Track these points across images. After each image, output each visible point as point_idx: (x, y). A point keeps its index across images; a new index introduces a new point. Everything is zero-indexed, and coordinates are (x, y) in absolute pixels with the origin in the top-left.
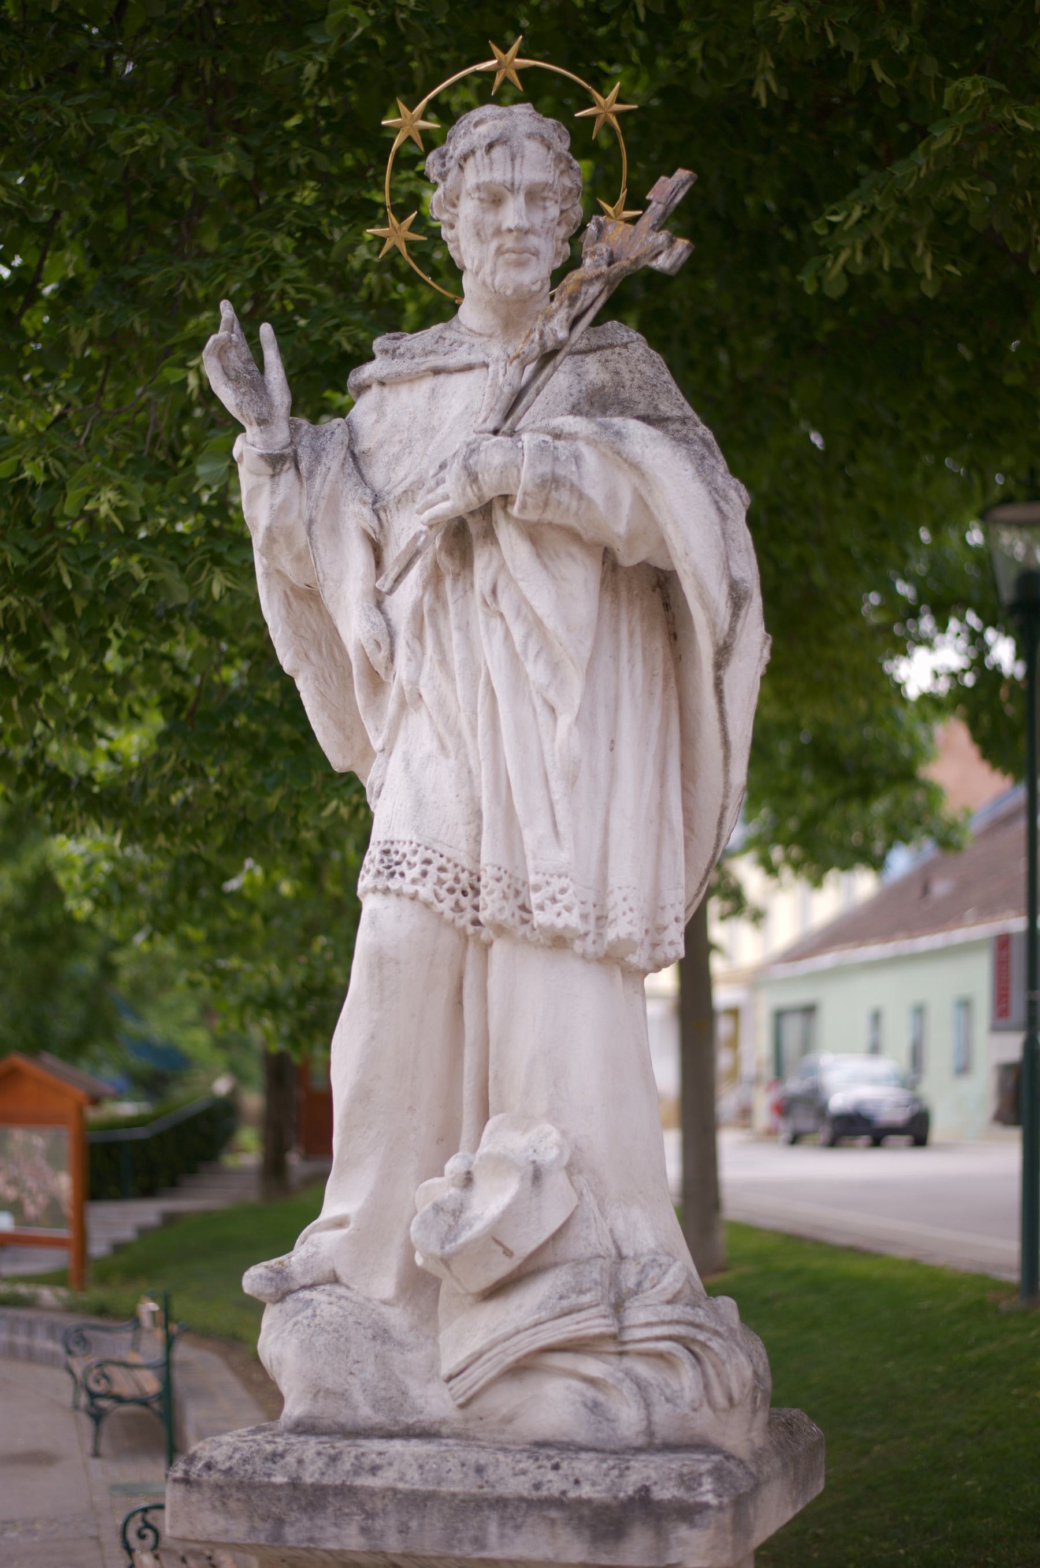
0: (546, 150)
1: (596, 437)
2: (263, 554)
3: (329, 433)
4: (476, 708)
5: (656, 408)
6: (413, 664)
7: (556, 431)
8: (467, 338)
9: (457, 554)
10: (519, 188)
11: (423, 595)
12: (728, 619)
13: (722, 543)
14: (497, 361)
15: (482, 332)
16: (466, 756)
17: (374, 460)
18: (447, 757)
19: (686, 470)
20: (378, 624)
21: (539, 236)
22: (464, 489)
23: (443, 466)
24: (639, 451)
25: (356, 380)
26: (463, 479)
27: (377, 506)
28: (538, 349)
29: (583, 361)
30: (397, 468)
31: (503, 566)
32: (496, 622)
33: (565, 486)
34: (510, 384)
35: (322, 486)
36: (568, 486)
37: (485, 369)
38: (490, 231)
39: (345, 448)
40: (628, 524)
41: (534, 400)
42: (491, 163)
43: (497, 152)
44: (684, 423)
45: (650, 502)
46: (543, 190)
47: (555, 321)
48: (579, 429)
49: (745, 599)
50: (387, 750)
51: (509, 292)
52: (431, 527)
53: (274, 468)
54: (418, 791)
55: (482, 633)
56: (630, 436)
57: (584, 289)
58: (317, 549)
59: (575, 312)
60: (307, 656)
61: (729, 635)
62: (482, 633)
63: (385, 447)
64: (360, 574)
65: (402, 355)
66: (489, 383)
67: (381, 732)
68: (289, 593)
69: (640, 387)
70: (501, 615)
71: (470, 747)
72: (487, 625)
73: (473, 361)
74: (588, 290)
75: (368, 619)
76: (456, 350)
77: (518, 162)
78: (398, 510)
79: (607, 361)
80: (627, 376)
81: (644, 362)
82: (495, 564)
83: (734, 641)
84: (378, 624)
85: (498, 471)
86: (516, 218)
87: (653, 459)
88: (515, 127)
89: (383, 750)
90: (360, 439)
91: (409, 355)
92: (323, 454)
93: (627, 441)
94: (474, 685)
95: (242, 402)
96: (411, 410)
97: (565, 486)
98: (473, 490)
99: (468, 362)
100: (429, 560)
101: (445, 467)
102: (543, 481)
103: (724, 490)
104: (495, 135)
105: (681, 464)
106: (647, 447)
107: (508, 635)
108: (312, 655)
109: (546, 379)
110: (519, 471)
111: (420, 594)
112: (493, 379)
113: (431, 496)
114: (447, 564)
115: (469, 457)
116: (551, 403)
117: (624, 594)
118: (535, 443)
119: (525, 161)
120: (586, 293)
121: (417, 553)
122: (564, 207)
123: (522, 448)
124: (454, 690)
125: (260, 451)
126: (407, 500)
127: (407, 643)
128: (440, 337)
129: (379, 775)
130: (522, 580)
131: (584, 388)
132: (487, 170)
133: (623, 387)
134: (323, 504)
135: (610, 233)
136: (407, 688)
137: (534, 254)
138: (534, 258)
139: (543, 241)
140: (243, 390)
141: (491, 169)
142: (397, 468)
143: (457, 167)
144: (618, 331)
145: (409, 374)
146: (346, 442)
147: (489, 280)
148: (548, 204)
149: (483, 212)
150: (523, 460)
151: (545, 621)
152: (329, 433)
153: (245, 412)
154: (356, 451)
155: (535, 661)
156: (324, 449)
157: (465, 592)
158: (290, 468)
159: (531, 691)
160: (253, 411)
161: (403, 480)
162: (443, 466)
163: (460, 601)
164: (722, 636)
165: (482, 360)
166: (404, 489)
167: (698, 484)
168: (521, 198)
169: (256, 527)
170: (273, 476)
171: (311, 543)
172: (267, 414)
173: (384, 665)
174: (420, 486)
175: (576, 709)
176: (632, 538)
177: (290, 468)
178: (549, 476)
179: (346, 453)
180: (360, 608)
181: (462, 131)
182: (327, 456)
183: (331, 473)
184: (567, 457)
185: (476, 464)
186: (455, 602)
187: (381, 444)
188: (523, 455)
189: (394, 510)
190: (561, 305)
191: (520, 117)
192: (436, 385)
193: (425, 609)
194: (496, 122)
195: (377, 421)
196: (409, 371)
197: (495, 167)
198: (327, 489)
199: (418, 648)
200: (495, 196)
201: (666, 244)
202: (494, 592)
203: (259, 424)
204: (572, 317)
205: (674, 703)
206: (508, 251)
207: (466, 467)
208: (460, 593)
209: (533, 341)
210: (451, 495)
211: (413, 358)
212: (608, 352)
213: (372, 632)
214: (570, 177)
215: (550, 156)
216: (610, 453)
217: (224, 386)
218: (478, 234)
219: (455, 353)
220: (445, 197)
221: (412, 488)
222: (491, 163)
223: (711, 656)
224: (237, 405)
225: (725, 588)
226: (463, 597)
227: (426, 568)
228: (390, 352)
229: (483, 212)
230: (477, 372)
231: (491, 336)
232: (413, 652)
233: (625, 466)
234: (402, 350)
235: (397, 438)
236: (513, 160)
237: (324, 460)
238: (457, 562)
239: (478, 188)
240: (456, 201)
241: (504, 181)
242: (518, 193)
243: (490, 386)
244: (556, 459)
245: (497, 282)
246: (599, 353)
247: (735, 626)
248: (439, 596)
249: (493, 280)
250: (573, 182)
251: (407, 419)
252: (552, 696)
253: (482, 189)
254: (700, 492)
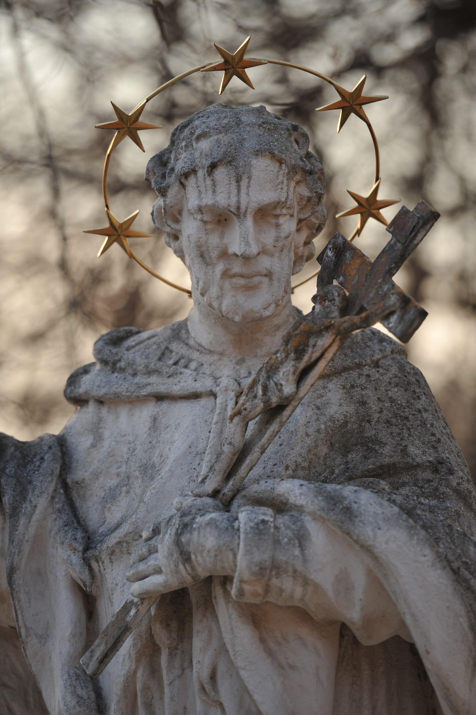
0: (278, 164)
1: (323, 514)
5: (404, 451)
8: (195, 355)
9: (174, 625)
10: (246, 211)
11: (137, 668)
14: (226, 390)
15: (212, 349)
19: (425, 556)
21: (272, 256)
22: (176, 566)
23: (156, 532)
24: (371, 534)
26: (175, 556)
27: (89, 554)
28: (262, 405)
29: (324, 388)
30: (113, 508)
33: (286, 572)
34: (230, 444)
35: (27, 528)
36: (290, 573)
37: (212, 398)
38: (214, 254)
39: (55, 479)
40: (362, 609)
41: (258, 459)
44: (436, 471)
46: (275, 208)
47: (281, 374)
48: (304, 503)
52: (142, 600)
56: (361, 513)
57: (312, 342)
58: (19, 601)
59: (302, 365)
63: (101, 479)
64: (67, 634)
65: (122, 370)
66: (215, 418)
69: (388, 422)
70: (221, 704)
74: (316, 342)
75: (74, 693)
76: (181, 373)
77: (244, 183)
78: (111, 562)
79: (352, 387)
80: (374, 406)
81: (397, 385)
84: (86, 697)
85: (212, 554)
86: (243, 244)
87: (387, 543)
88: (241, 142)
90: (74, 464)
91: (130, 371)
92: (30, 487)
93: (357, 520)
96: (131, 438)
98: (186, 569)
99: (194, 390)
101: (159, 533)
102: (261, 569)
104: (218, 155)
106: (379, 529)
109: (271, 436)
110: (235, 555)
111: (134, 667)
113: (142, 567)
115: (181, 534)
116: (284, 444)
119: (252, 182)
120: (314, 346)
123: (238, 530)
126: (122, 552)
128: (167, 348)
130: (243, 669)
131: (323, 426)
133: (369, 421)
137: (265, 276)
138: (265, 280)
139: (276, 260)
141: (214, 192)
142: (113, 508)
143: (178, 184)
144: (370, 343)
145: (129, 397)
146: (57, 472)
147: (215, 304)
148: (282, 220)
149: (207, 234)
150: (239, 544)
152: (38, 457)
154: (69, 481)
156: (30, 482)
157: (183, 670)
161: (118, 526)
162: (156, 532)
163: (177, 682)
165: (209, 389)
166: (118, 540)
167: (439, 571)
168: (249, 222)
171: (12, 594)
174: (136, 537)
178: (268, 563)
180: (66, 677)
181: (184, 144)
182: (33, 492)
183: (37, 511)
186: (171, 684)
188: (239, 537)
189: (107, 561)
190: (287, 357)
192: (158, 412)
193: (139, 686)
194: (220, 136)
195: (93, 446)
197: (219, 189)
200: (220, 215)
201: (398, 304)
202: (213, 677)
204: (299, 370)
206: (234, 276)
207: (177, 543)
209: (255, 397)
210: (163, 569)
212: (355, 374)
213: (78, 708)
214: (307, 185)
215: (282, 172)
216: (339, 532)
218: (202, 256)
219: (179, 377)
227: (141, 637)
228: (110, 364)
229: (207, 234)
230: (203, 401)
231: (222, 354)
233: (357, 547)
234: (122, 364)
236: (238, 181)
237: (30, 496)
239: (200, 210)
242: (245, 216)
243: (216, 423)
244: (277, 542)
246: (345, 375)
249: (220, 305)
250: (311, 190)
253: (204, 212)
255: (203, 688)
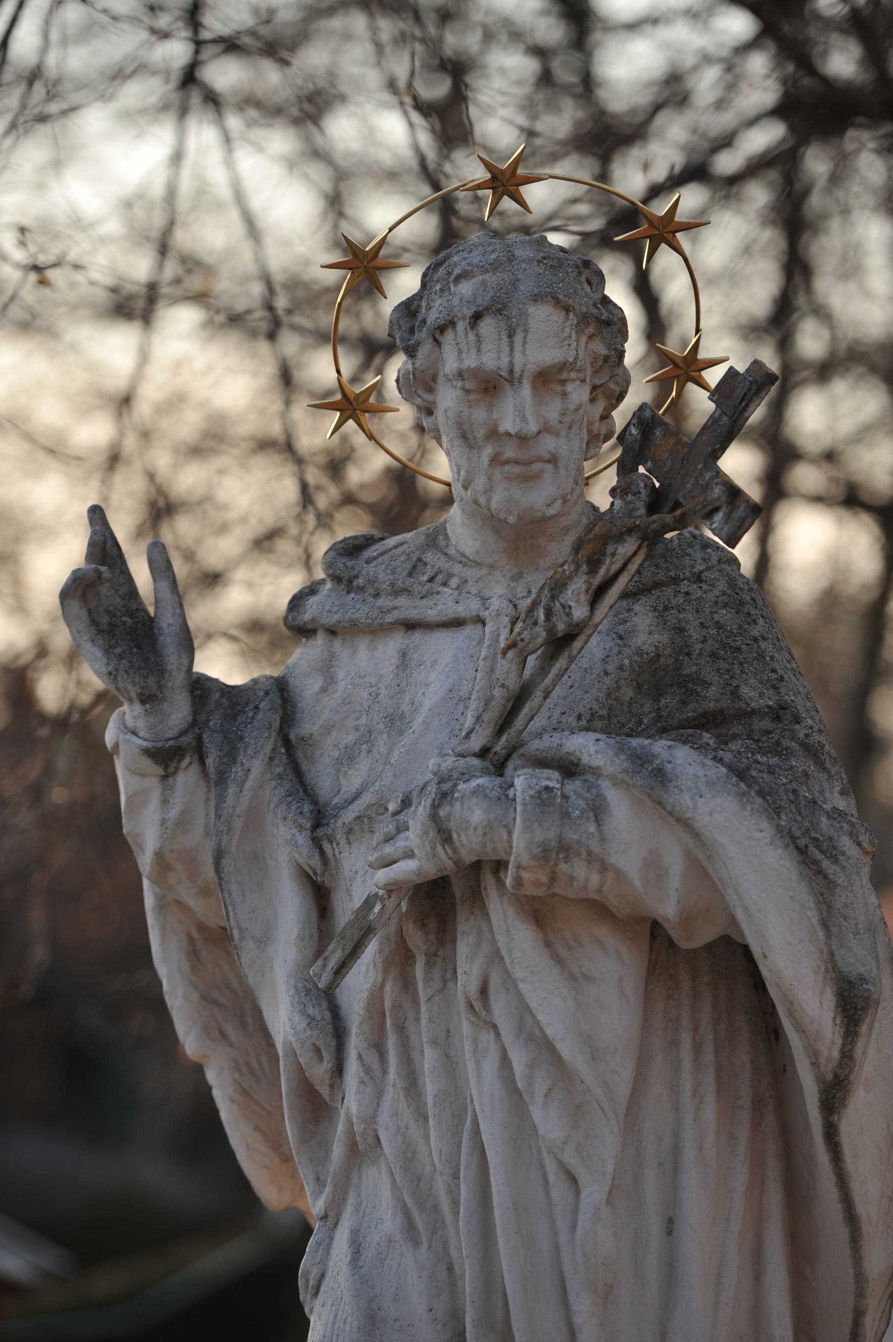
1: (626, 778)
2: (153, 882)
3: (251, 706)
4: (459, 1169)
5: (735, 693)
6: (368, 1090)
7: (572, 758)
8: (457, 568)
9: (432, 924)
12: (839, 1042)
13: (821, 935)
14: (498, 615)
15: (479, 561)
16: (445, 1244)
17: (318, 753)
18: (416, 1243)
19: (761, 831)
20: (319, 1017)
21: (557, 435)
22: (433, 848)
24: (690, 803)
25: (293, 620)
27: (320, 832)
28: (544, 634)
29: (628, 610)
30: (350, 772)
31: (496, 956)
32: (487, 1038)
33: (578, 854)
36: (584, 855)
37: (480, 626)
38: (480, 433)
42: (479, 341)
43: (487, 326)
45: (710, 871)
47: (569, 592)
48: (601, 764)
49: (865, 1009)
50: (332, 1217)
51: (511, 519)
52: (390, 892)
53: (166, 767)
54: (371, 1301)
55: (468, 1054)
57: (610, 549)
58: (230, 894)
59: (597, 580)
60: (223, 1034)
61: (841, 1065)
62: (468, 1054)
63: (334, 734)
64: (293, 937)
65: (361, 589)
67: (324, 1185)
68: (195, 934)
69: (713, 655)
70: (495, 1027)
71: (451, 1230)
72: (475, 1042)
73: (463, 615)
74: (616, 549)
75: (304, 1013)
77: (518, 338)
78: (349, 843)
80: (695, 633)
82: (485, 948)
83: (852, 1070)
84: (319, 1017)
86: (518, 419)
87: (711, 815)
89: (324, 1217)
90: (299, 715)
91: (371, 591)
92: (241, 745)
93: (672, 785)
94: (457, 1134)
95: (117, 670)
96: (373, 680)
97: (578, 854)
100: (392, 928)
101: (410, 805)
102: (544, 851)
103: (831, 838)
104: (483, 301)
105: (753, 822)
107: (505, 1061)
108: (231, 1031)
110: (510, 833)
112: (490, 646)
113: (388, 849)
114: (416, 940)
116: (576, 685)
117: (686, 985)
118: (532, 792)
119: (529, 336)
120: (613, 554)
121: (368, 932)
122: (597, 382)
123: (514, 800)
124: (427, 1138)
125: (145, 744)
127: (360, 1056)
128: (419, 559)
129: (317, 1259)
130: (523, 981)
131: (626, 662)
132: (473, 351)
133: (688, 654)
134: (238, 825)
135: (658, 442)
136: (358, 1128)
137: (549, 461)
138: (549, 467)
139: (563, 440)
140: (118, 650)
141: (479, 350)
143: (430, 340)
146: (276, 725)
147: (482, 500)
148: (569, 387)
149: (470, 407)
150: (515, 819)
151: (559, 1045)
152: (251, 706)
153: (121, 685)
154: (292, 737)
155: (545, 1104)
156: (241, 739)
158: (190, 763)
159: (540, 1148)
160: (134, 684)
161: (357, 796)
162: (406, 803)
163: (437, 998)
164: (830, 1068)
167: (780, 851)
168: (526, 390)
169: (142, 849)
170: (165, 777)
172: (154, 687)
173: (327, 1082)
175: (609, 1179)
176: (687, 918)
177: (190, 763)
179: (276, 740)
181: (438, 287)
182: (245, 751)
183: (251, 777)
184: (582, 812)
185: (449, 815)
187: (328, 729)
188: (515, 810)
189: (343, 842)
191: (523, 266)
192: (408, 645)
193: (387, 1004)
194: (487, 276)
195: (324, 690)
196: (369, 621)
197: (485, 347)
198: (245, 801)
199: (376, 1065)
202: (484, 991)
203: (143, 702)
205: (772, 1147)
206: (508, 462)
207: (434, 817)
208: (437, 985)
209: (535, 623)
210: (416, 852)
211: (377, 596)
212: (669, 591)
215: (569, 323)
217: (90, 644)
218: (464, 436)
220: (415, 378)
221: (369, 813)
222: (479, 341)
223: (817, 1096)
224: (110, 674)
225: (830, 999)
226: (440, 991)
227: (389, 940)
229: (470, 407)
230: (468, 630)
231: (492, 567)
232: (367, 1070)
233: (672, 821)
234: (360, 581)
235: (350, 723)
236: (511, 335)
238: (432, 937)
240: (432, 384)
241: (499, 368)
242: (520, 382)
243: (485, 659)
245: (494, 505)
247: (852, 1050)
248: (407, 984)
249: (489, 501)
251: (365, 695)
252: (570, 1158)
253: (465, 377)
254: (782, 862)
255: (471, 1006)
